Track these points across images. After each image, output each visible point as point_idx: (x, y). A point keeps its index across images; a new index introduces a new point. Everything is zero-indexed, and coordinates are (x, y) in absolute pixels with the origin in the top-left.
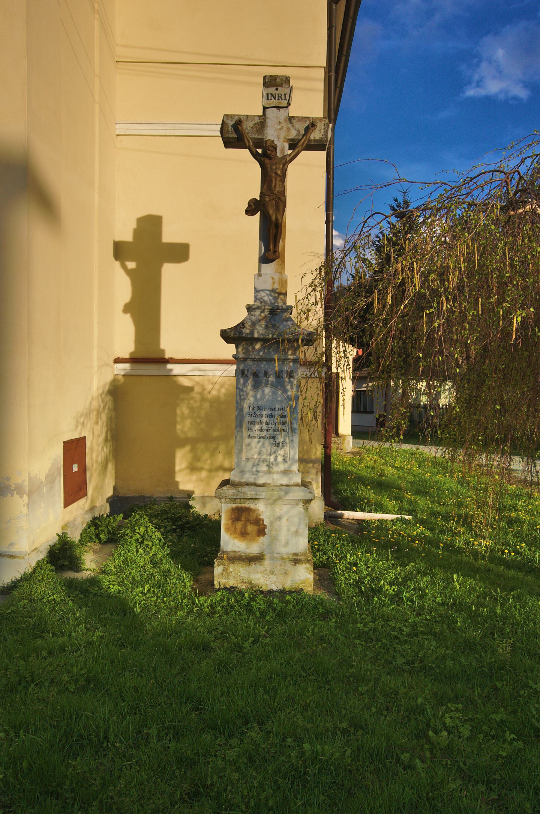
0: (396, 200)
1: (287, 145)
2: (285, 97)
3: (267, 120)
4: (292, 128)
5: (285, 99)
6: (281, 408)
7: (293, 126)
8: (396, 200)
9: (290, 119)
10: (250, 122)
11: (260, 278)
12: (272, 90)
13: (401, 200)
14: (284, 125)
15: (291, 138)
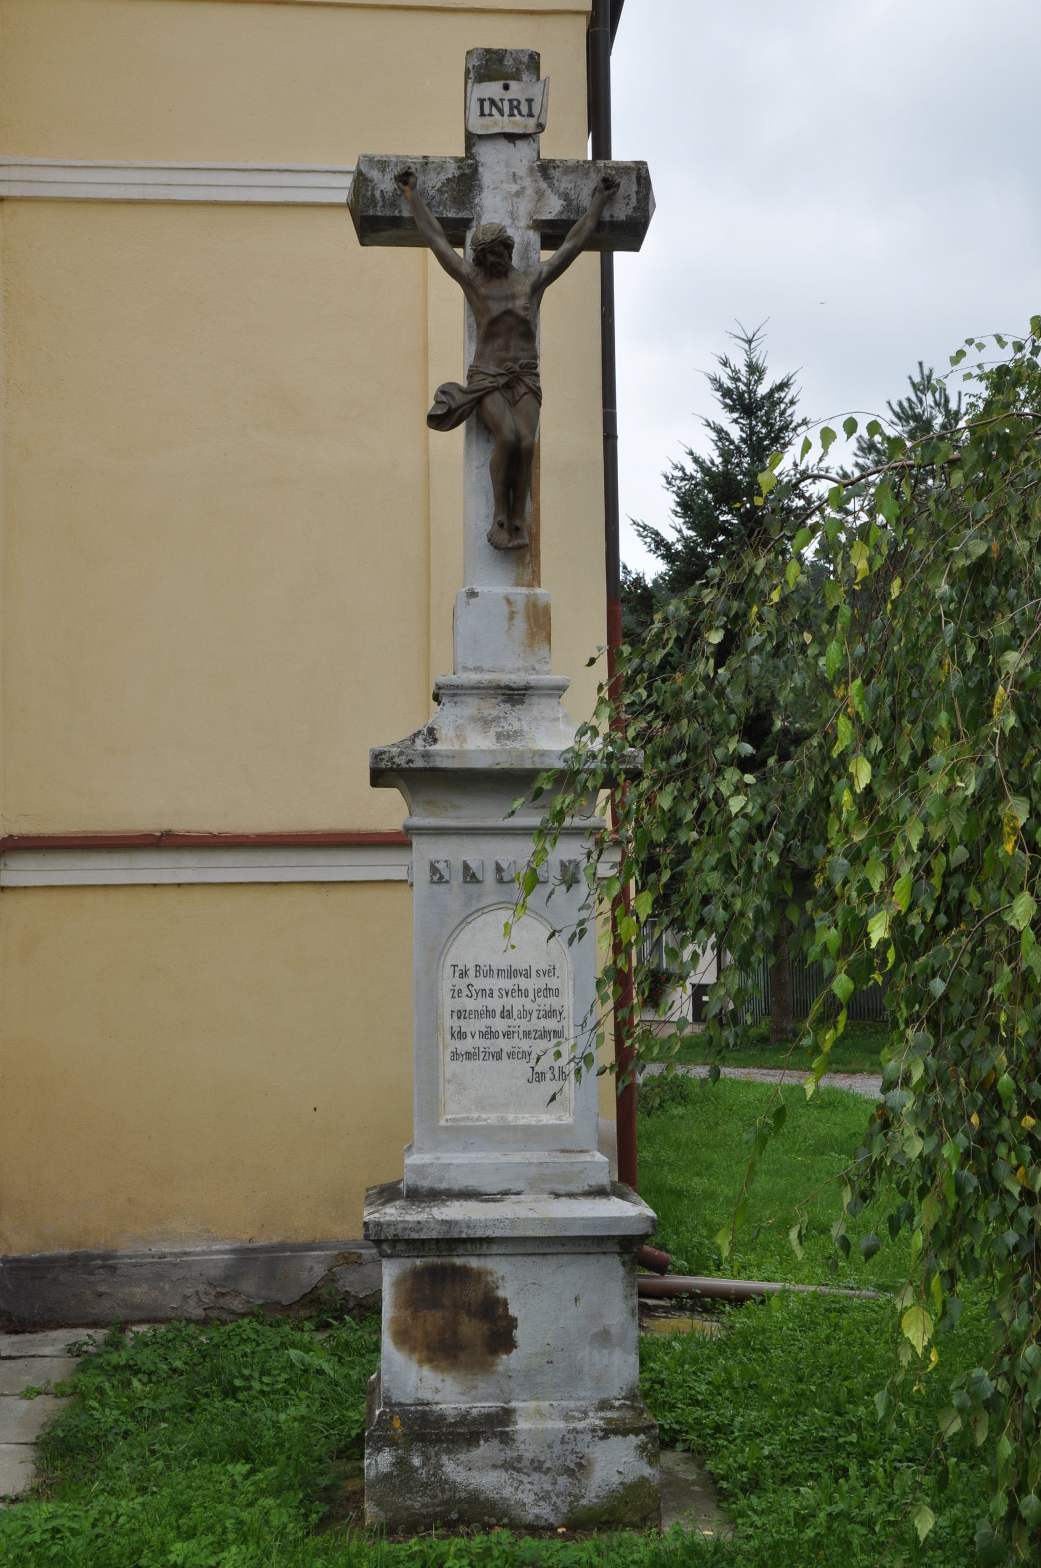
0: (725, 363)
1: (534, 237)
2: (530, 107)
3: (481, 169)
4: (549, 192)
5: (531, 115)
6: (546, 967)
7: (551, 186)
8: (725, 363)
9: (545, 169)
10: (433, 175)
11: (472, 601)
12: (493, 89)
13: (740, 363)
14: (527, 182)
15: (549, 217)
